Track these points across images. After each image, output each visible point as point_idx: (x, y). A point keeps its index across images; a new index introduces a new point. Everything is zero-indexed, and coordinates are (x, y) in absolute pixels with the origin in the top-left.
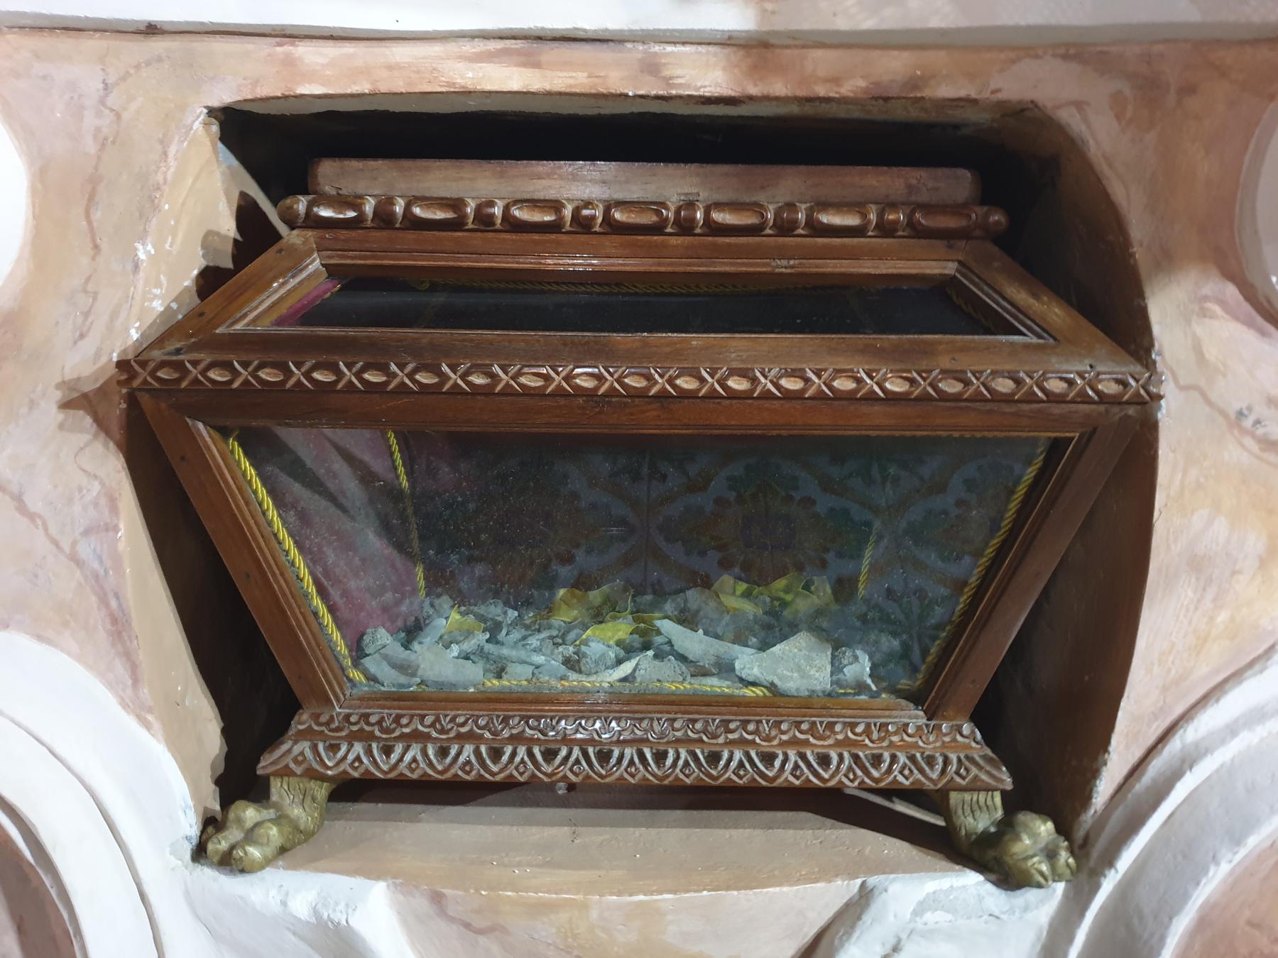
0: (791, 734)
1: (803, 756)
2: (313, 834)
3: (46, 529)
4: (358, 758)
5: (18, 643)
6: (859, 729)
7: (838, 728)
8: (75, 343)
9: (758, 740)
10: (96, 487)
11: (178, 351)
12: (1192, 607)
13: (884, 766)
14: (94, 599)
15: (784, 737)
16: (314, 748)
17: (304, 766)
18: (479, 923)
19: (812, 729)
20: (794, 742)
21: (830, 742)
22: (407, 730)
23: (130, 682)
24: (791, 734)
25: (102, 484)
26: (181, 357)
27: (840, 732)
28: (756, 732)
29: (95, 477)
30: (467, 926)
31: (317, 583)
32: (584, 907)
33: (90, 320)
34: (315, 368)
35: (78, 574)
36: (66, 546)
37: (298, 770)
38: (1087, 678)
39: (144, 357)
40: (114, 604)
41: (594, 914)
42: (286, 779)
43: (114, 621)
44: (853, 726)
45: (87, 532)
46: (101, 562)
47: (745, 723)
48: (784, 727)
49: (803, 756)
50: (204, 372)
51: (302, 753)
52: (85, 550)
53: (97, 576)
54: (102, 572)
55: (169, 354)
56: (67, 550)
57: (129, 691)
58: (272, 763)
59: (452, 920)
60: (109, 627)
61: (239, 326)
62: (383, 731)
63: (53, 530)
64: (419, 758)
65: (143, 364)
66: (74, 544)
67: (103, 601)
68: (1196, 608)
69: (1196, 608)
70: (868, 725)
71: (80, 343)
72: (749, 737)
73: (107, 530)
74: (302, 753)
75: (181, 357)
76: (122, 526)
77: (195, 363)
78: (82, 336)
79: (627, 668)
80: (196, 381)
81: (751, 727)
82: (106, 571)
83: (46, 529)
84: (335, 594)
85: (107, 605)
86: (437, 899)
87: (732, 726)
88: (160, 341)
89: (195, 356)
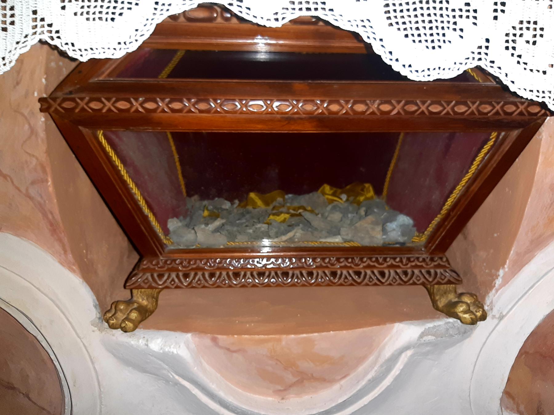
0: (367, 263)
1: (373, 272)
2: (152, 312)
3: (12, 182)
4: (173, 280)
5: (9, 239)
6: (398, 260)
7: (388, 260)
8: (15, 87)
9: (353, 266)
10: (34, 161)
11: (71, 93)
12: (549, 207)
13: (409, 276)
14: (40, 215)
15: (365, 264)
16: (152, 276)
17: (148, 285)
18: (233, 348)
19: (377, 261)
20: (369, 266)
21: (385, 265)
22: (194, 266)
23: (63, 252)
24: (367, 263)
25: (37, 159)
26: (73, 96)
27: (390, 262)
28: (352, 262)
29: (33, 156)
30: (228, 349)
31: (147, 202)
32: (280, 340)
33: (21, 75)
34: (145, 101)
35: (31, 203)
36: (23, 189)
37: (146, 286)
38: (495, 235)
39: (54, 96)
40: (50, 217)
41: (284, 343)
42: (140, 290)
43: (52, 225)
44: (395, 259)
45: (33, 183)
46: (42, 197)
47: (347, 259)
48: (365, 259)
49: (373, 272)
50: (87, 104)
51: (147, 279)
52: (33, 192)
53: (40, 204)
54: (42, 202)
55: (67, 94)
56: (24, 191)
57: (63, 256)
58: (133, 284)
59: (221, 347)
60: (49, 227)
61: (101, 78)
62: (183, 267)
63: (16, 183)
64: (202, 278)
65: (54, 99)
66: (27, 190)
67: (45, 215)
68: (550, 207)
69: (550, 207)
70: (401, 259)
71: (17, 87)
72: (349, 265)
73: (43, 182)
74: (147, 279)
75: (73, 96)
76: (50, 179)
77: (82, 99)
78: (18, 83)
79: (290, 235)
80: (83, 109)
81: (350, 260)
82: (45, 201)
83: (12, 182)
84: (156, 208)
85: (48, 218)
86: (214, 340)
87: (342, 260)
88: (60, 87)
89: (83, 95)
